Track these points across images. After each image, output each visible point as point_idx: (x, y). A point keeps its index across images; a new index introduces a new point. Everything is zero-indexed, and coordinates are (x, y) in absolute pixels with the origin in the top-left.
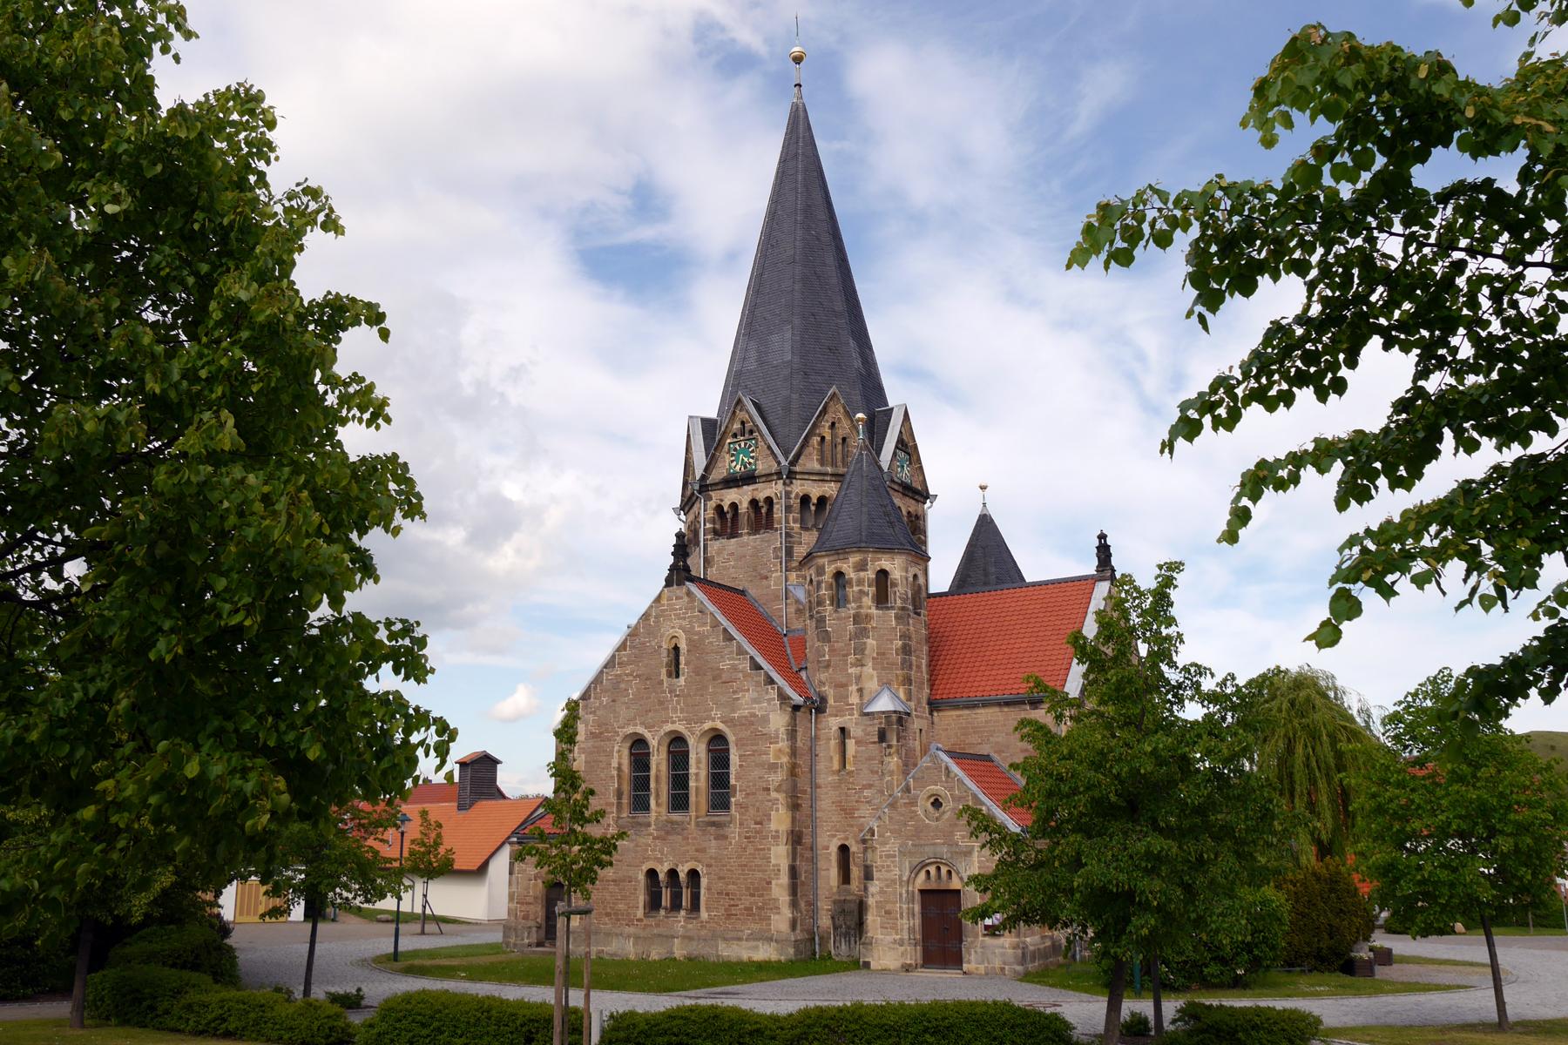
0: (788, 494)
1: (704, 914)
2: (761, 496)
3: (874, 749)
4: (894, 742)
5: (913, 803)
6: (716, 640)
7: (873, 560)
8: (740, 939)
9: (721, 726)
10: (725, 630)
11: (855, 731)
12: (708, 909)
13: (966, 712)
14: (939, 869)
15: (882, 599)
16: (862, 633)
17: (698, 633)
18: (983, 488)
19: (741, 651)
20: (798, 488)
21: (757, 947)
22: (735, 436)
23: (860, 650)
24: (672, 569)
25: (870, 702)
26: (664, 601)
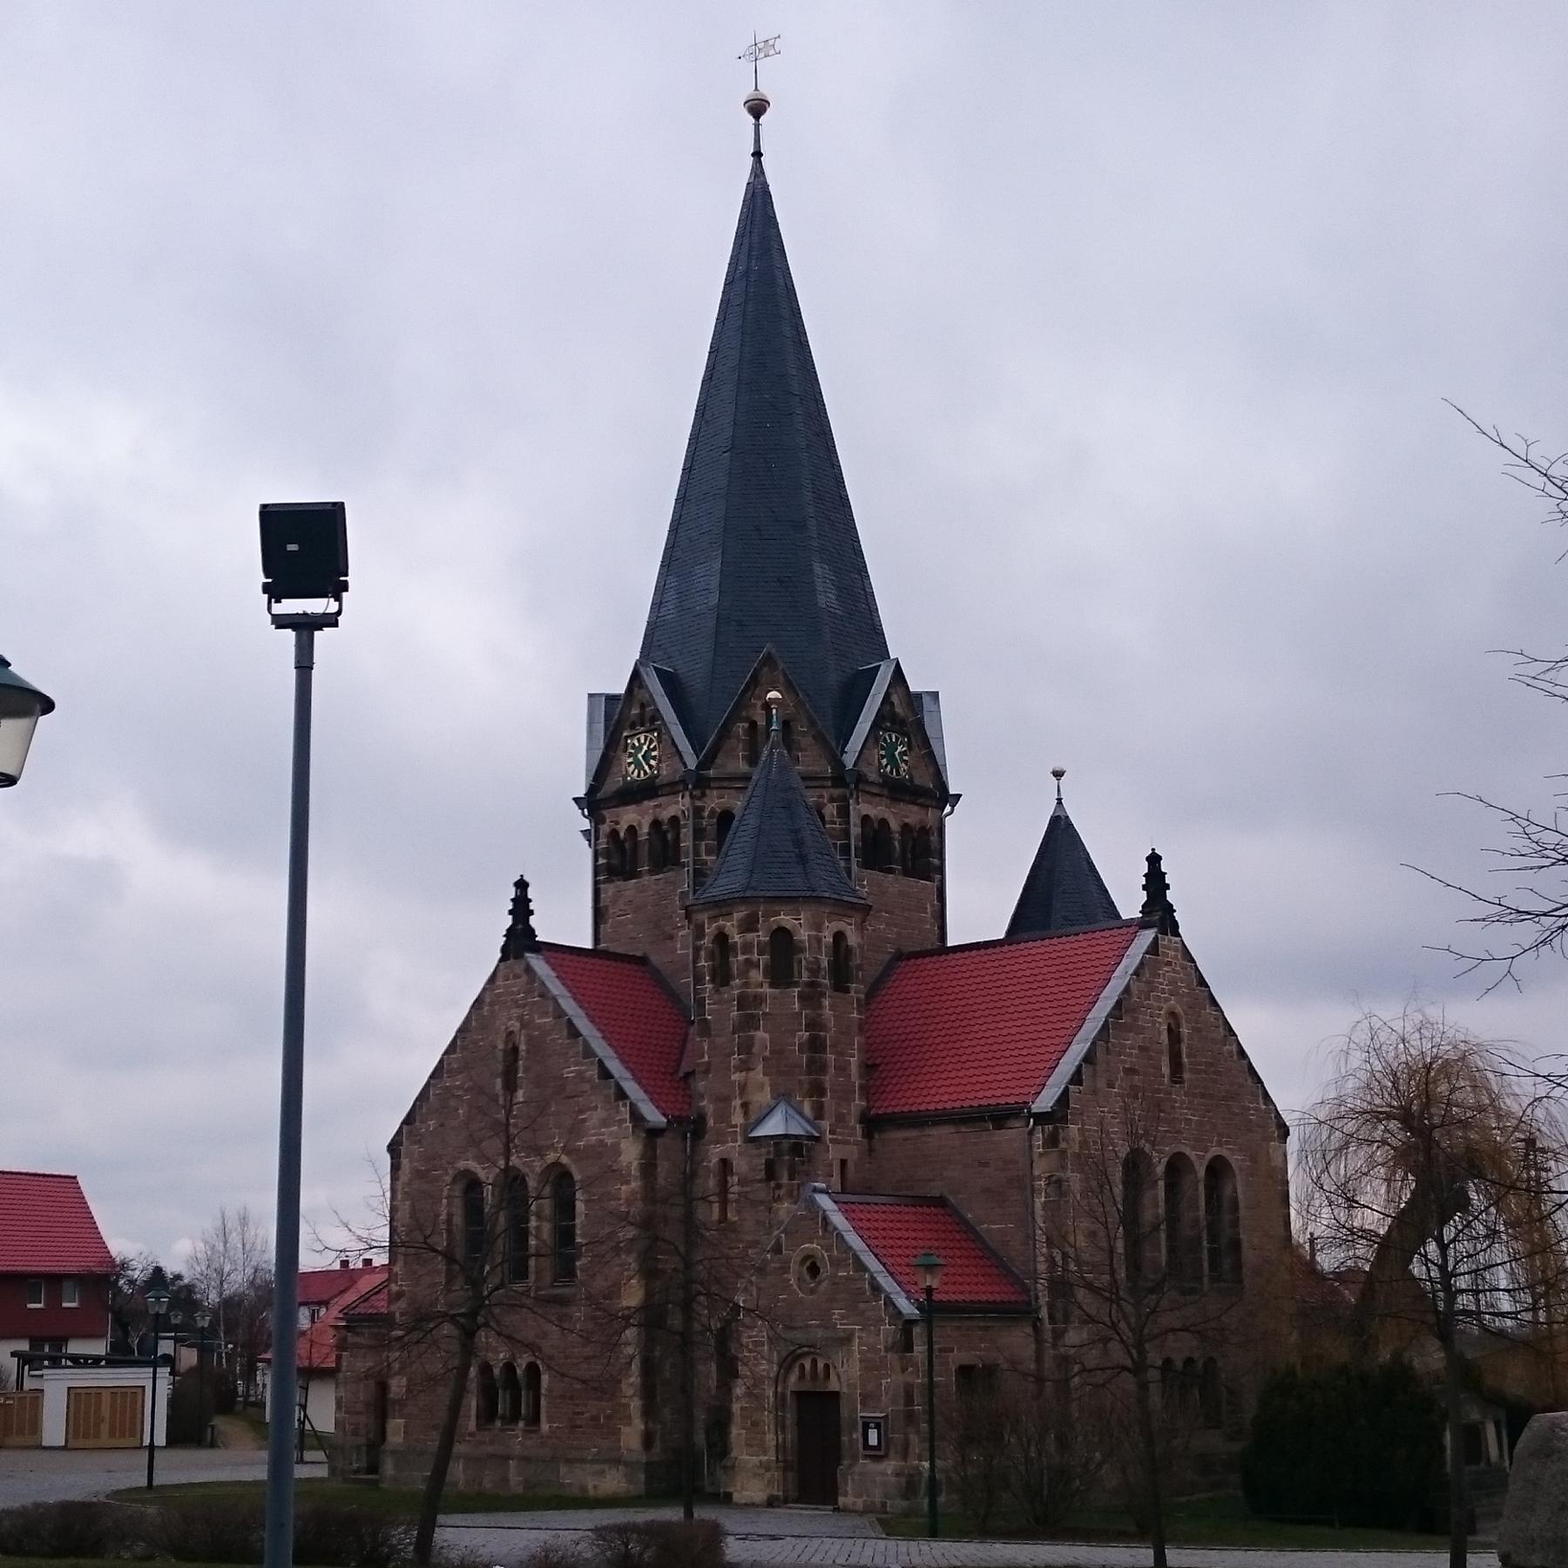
0: (698, 812)
1: (545, 1427)
2: (665, 815)
3: (761, 1192)
4: (785, 1180)
5: (786, 1269)
6: (559, 1037)
7: (767, 916)
8: (583, 1461)
9: (565, 1159)
10: (570, 1023)
11: (740, 1165)
12: (550, 1420)
13: (913, 1133)
14: (814, 1363)
15: (780, 974)
16: (749, 1023)
17: (539, 1027)
18: (1058, 774)
19: (588, 1052)
20: (714, 801)
21: (603, 1472)
22: (633, 726)
23: (746, 1047)
24: (510, 933)
25: (760, 1121)
26: (499, 982)
